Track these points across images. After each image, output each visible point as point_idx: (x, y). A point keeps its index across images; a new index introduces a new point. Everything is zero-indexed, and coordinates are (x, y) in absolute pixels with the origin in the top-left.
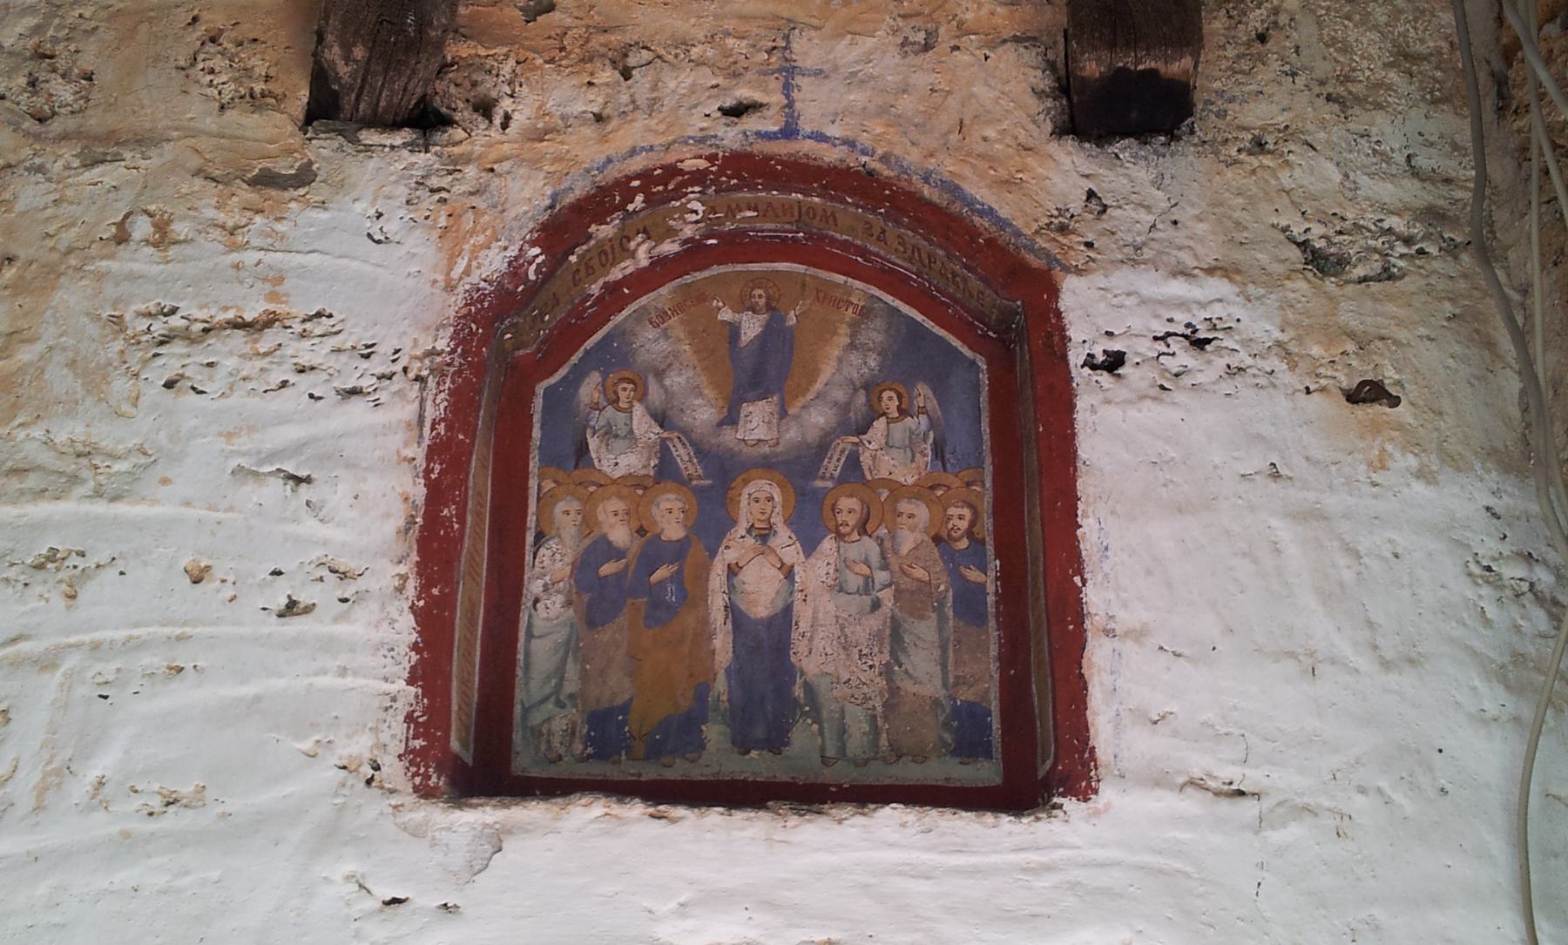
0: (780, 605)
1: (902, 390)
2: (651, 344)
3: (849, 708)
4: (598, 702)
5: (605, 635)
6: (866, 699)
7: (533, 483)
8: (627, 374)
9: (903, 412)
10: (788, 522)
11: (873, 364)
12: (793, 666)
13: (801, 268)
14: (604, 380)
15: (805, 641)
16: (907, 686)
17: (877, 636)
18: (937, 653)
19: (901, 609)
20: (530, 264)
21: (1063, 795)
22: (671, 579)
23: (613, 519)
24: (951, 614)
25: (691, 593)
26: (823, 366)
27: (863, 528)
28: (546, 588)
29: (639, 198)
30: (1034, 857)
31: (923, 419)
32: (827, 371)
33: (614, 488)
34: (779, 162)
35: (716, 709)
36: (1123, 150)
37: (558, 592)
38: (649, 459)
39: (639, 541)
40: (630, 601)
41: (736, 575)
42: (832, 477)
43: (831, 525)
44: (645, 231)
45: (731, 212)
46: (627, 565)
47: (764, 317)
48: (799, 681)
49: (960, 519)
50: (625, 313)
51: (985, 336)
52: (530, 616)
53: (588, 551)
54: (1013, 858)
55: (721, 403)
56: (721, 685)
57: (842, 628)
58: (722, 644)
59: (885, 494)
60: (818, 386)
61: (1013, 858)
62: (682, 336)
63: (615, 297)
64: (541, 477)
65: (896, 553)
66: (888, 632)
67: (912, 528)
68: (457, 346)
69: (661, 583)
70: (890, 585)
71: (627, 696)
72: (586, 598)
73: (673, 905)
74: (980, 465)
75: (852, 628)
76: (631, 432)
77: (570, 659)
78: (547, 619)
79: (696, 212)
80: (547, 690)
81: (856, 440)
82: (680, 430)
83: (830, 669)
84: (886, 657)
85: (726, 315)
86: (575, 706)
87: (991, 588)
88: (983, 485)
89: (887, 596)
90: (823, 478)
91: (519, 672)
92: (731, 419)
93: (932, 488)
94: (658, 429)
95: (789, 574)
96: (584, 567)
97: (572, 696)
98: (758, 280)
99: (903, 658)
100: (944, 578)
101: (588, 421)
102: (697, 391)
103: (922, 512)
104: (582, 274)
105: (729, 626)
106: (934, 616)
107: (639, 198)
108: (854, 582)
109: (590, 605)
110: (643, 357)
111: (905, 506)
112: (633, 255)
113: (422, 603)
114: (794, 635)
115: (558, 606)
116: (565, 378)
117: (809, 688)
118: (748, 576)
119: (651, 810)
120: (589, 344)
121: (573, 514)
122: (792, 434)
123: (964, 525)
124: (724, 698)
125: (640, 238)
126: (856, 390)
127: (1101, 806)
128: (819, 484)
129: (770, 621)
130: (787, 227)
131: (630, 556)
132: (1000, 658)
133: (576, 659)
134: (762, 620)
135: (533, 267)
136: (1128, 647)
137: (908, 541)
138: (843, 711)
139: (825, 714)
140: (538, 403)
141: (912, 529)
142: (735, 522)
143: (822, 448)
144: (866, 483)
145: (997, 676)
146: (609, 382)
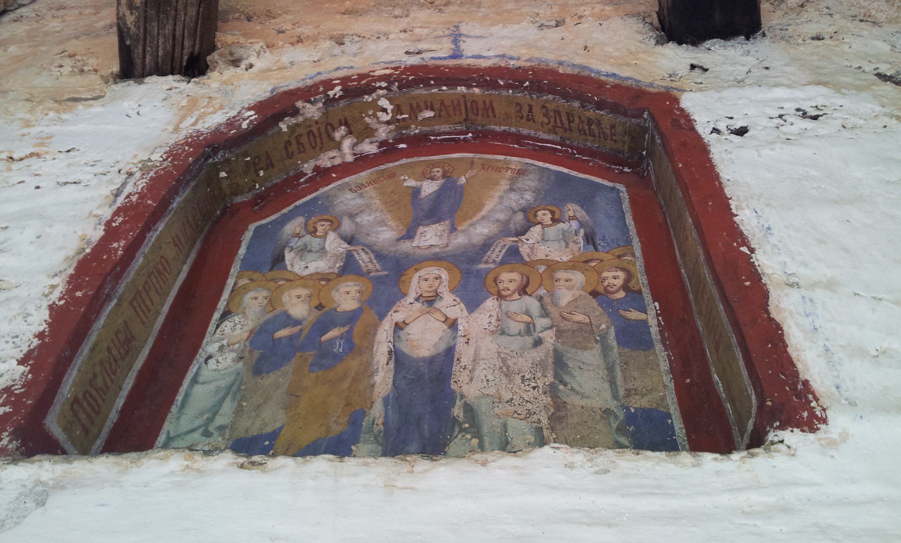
0: (442, 347)
1: (554, 209)
2: (347, 200)
3: (511, 422)
4: (247, 430)
5: (268, 380)
6: (530, 413)
7: (231, 282)
8: (325, 217)
9: (555, 221)
10: (453, 291)
11: (529, 198)
12: (453, 392)
13: (471, 155)
14: (307, 221)
15: (467, 372)
16: (574, 400)
17: (541, 365)
18: (603, 373)
19: (563, 343)
20: (244, 120)
21: (782, 427)
22: (341, 337)
23: (295, 300)
24: (615, 344)
25: (357, 346)
26: (487, 202)
27: (523, 290)
28: (221, 348)
29: (338, 88)
30: (756, 498)
31: (574, 224)
32: (489, 205)
33: (301, 282)
34: (446, 68)
35: (370, 431)
36: (712, 45)
37: (233, 351)
38: (336, 262)
39: (316, 313)
41: (402, 329)
42: (494, 261)
43: (494, 290)
44: (346, 124)
45: (415, 111)
46: (301, 330)
47: (440, 182)
48: (458, 403)
49: (614, 278)
50: (330, 187)
51: (622, 172)
52: (199, 368)
53: (267, 323)
54: (727, 500)
55: (401, 228)
56: (377, 411)
57: (504, 361)
58: (383, 379)
59: (542, 269)
60: (484, 212)
61: (727, 500)
62: (374, 195)
63: (323, 175)
64: (239, 277)
65: (555, 304)
66: (551, 361)
67: (570, 289)
68: (168, 157)
69: (332, 341)
70: (551, 328)
71: (278, 425)
72: (257, 354)
74: (629, 243)
75: (514, 360)
76: (323, 248)
77: (228, 400)
78: (215, 370)
79: (384, 110)
80: (198, 422)
81: (516, 239)
82: (364, 245)
83: (492, 391)
84: (550, 379)
85: (411, 183)
86: (222, 435)
87: (653, 322)
88: (633, 255)
89: (549, 337)
90: (486, 262)
91: (174, 409)
92: (410, 235)
93: (587, 262)
94: (346, 245)
95: (453, 325)
96: (261, 337)
97: (221, 428)
98: (435, 164)
99: (567, 378)
100: (605, 318)
101: (287, 243)
102: (382, 223)
103: (578, 278)
104: (294, 147)
105: (392, 365)
106: (598, 346)
107: (338, 88)
108: (515, 327)
109: (259, 360)
110: (340, 208)
111: (561, 275)
112: (338, 146)
113: (62, 302)
114: (456, 368)
115: (229, 360)
116: (274, 221)
117: (469, 409)
118: (414, 331)
119: (242, 460)
120: (298, 203)
121: (260, 300)
122: (460, 240)
123: (619, 282)
124: (380, 421)
125: (343, 130)
126: (514, 212)
127: (834, 436)
128: (482, 266)
129: (432, 360)
131: (305, 323)
132: (672, 370)
133: (234, 399)
134: (424, 360)
135: (248, 121)
136: (819, 294)
137: (565, 297)
138: (505, 426)
139: (485, 429)
140: (248, 235)
141: (570, 288)
142: (405, 295)
143: (487, 245)
144: (525, 263)
145: (672, 385)
146: (311, 222)
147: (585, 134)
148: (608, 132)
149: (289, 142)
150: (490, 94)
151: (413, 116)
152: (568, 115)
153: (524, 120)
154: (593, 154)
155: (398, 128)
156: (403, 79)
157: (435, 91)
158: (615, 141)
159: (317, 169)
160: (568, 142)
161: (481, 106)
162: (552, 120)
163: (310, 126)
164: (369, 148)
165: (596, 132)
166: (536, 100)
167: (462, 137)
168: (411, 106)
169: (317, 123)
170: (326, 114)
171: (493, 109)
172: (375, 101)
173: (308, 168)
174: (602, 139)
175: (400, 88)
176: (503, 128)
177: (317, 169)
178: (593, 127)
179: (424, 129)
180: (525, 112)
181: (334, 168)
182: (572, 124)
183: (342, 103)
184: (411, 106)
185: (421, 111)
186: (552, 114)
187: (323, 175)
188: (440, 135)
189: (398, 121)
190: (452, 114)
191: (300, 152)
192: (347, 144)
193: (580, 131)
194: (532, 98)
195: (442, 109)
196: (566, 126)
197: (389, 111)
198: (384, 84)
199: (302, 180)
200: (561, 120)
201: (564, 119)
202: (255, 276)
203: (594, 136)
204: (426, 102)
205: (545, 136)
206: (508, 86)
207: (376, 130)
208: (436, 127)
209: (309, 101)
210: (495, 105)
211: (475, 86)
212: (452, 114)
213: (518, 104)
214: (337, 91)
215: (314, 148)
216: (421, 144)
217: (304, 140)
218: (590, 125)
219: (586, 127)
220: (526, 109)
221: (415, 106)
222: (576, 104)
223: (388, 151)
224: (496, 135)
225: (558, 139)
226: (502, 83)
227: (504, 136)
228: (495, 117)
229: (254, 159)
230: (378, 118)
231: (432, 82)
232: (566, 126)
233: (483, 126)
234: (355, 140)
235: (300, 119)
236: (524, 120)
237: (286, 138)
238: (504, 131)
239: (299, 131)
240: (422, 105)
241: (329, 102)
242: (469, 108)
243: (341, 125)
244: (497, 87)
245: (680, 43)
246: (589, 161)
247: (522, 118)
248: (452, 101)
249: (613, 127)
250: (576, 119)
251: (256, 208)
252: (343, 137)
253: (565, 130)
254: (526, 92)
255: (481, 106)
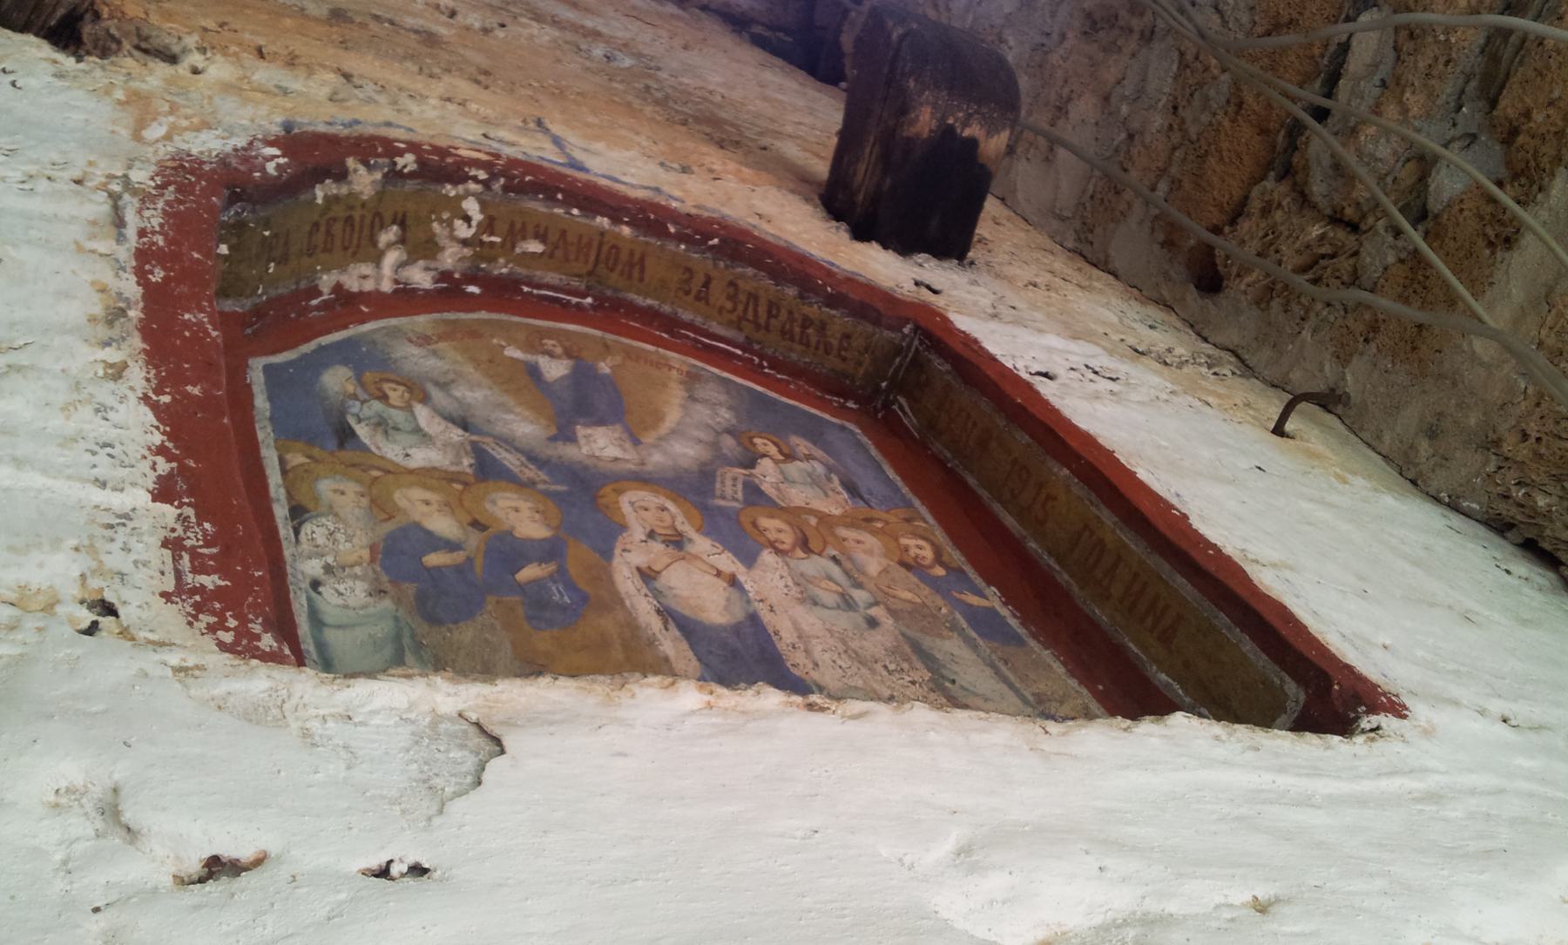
40: (491, 599)
44: (402, 224)
45: (515, 234)
51: (843, 407)
73: (944, 848)
79: (467, 219)
98: (550, 334)
99: (945, 672)
112: (377, 259)
120: (326, 340)
130: (575, 283)
147: (792, 339)
148: (835, 343)
149: (316, 225)
150: (647, 243)
151: (509, 245)
152: (771, 304)
153: (690, 298)
154: (797, 372)
155: (478, 257)
156: (514, 177)
157: (559, 211)
158: (844, 359)
159: (338, 288)
160: (756, 347)
161: (624, 257)
162: (741, 308)
163: (352, 208)
164: (420, 277)
165: (814, 340)
166: (722, 271)
167: (575, 300)
168: (512, 225)
169: (363, 205)
170: (380, 195)
171: (642, 270)
172: (460, 198)
173: (326, 281)
174: (821, 351)
175: (506, 189)
176: (649, 302)
177: (338, 288)
178: (810, 331)
179: (519, 270)
180: (696, 285)
181: (361, 296)
182: (773, 321)
183: (410, 185)
184: (512, 225)
185: (524, 238)
186: (743, 297)
187: (348, 305)
188: (539, 287)
189: (482, 243)
190: (572, 257)
191: (325, 250)
192: (392, 258)
193: (783, 332)
194: (716, 266)
195: (559, 244)
196: (762, 321)
197: (474, 223)
198: (482, 175)
199: (314, 302)
200: (756, 311)
201: (762, 310)
202: (316, 452)
203: (808, 345)
204: (538, 226)
205: (721, 331)
206: (680, 238)
207: (443, 249)
208: (538, 273)
209: (366, 163)
210: (649, 262)
211: (627, 223)
212: (572, 257)
213: (688, 270)
214: (408, 162)
215: (346, 249)
216: (503, 293)
217: (337, 228)
218: (804, 327)
219: (797, 330)
220: (699, 279)
221: (518, 226)
222: (791, 291)
223: (449, 292)
224: (634, 311)
225: (741, 338)
226: (672, 230)
227: (650, 316)
228: (641, 280)
229: (275, 236)
230: (452, 230)
231: (560, 196)
232: (762, 321)
233: (616, 290)
234: (405, 257)
235: (344, 190)
236: (690, 298)
237: (316, 217)
238: (650, 307)
239: (339, 211)
240: (530, 229)
241: (394, 175)
242: (603, 256)
243: (394, 222)
244: (665, 234)
245: (886, 247)
246: (789, 383)
247: (687, 293)
248: (580, 237)
249: (847, 336)
250: (784, 314)
251: (249, 331)
252: (390, 245)
253: (758, 327)
254: (708, 255)
255: (624, 257)
